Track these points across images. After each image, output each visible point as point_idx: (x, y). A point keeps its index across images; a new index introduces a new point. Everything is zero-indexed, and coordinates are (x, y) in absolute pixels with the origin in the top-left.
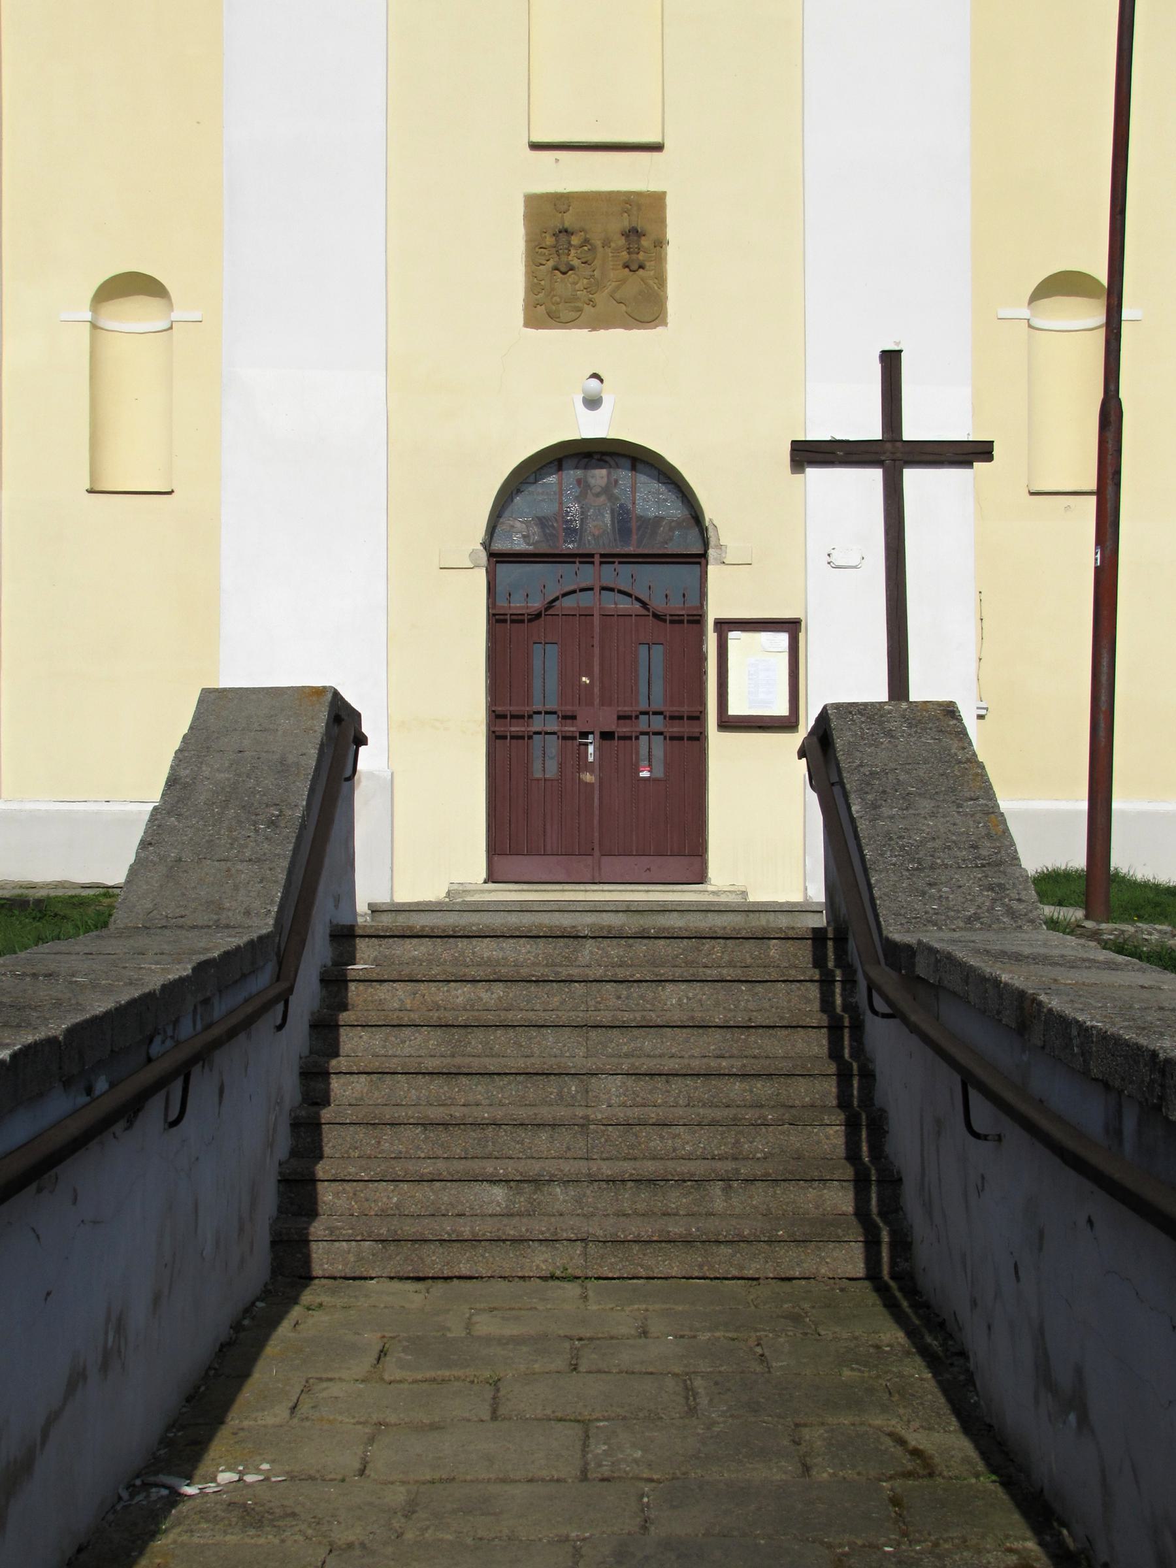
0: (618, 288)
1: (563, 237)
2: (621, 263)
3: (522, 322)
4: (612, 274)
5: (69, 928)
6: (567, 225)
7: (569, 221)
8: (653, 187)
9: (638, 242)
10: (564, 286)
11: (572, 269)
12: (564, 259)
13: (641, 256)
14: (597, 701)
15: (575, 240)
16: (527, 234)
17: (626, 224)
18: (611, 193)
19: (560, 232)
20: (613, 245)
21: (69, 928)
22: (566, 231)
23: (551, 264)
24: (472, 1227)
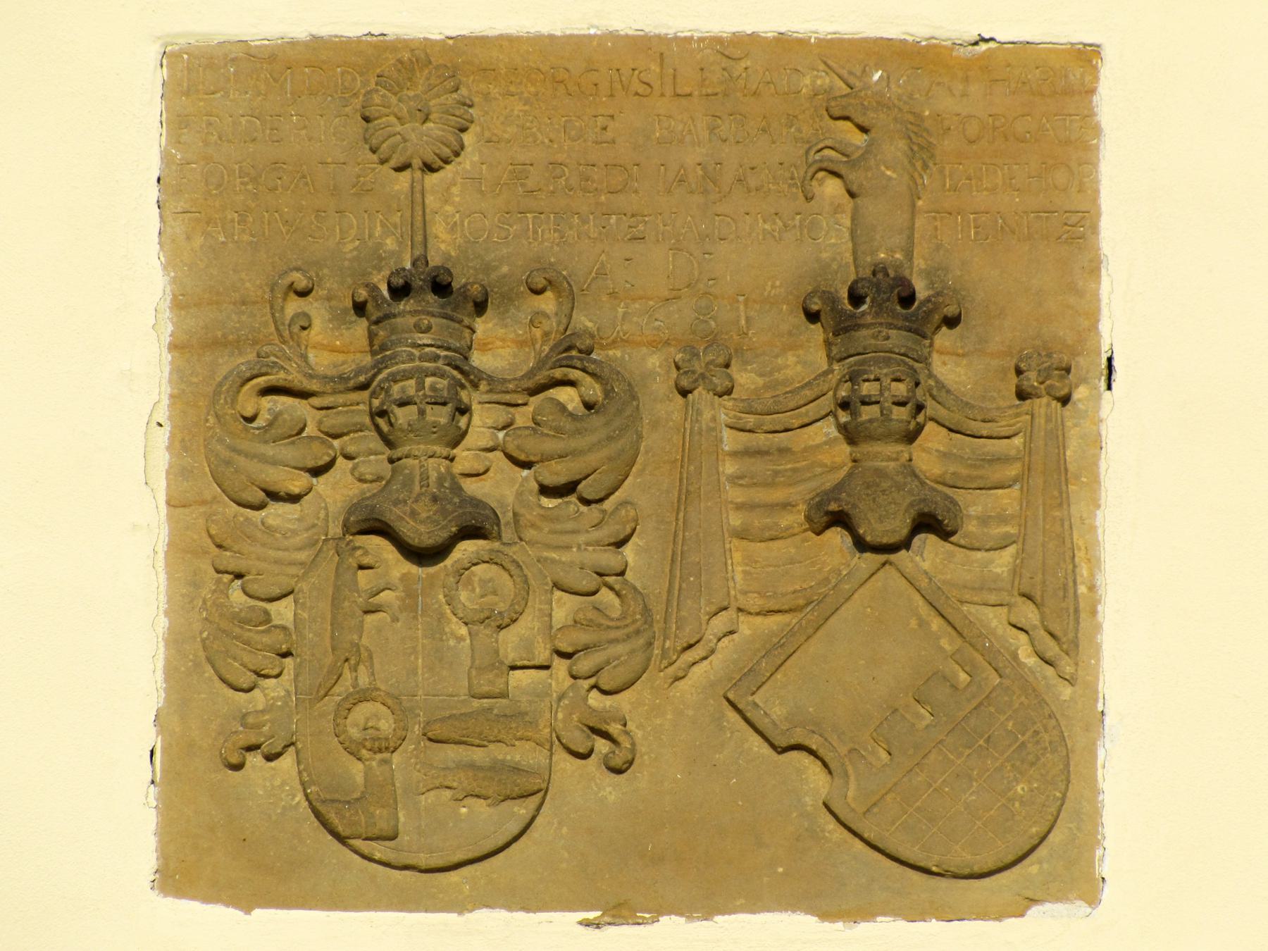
0: (779, 652)
1: (419, 325)
2: (801, 493)
3: (141, 848)
4: (739, 568)
5: (368, 744)
6: (444, 245)
7: (457, 220)
8: (134, 142)
9: (913, 368)
10: (425, 633)
12: (425, 461)
13: (932, 452)
15: (498, 347)
16: (181, 303)
18: (732, 50)
19: (400, 291)
20: (745, 378)
21: (368, 744)
22: (441, 287)
23: (336, 492)
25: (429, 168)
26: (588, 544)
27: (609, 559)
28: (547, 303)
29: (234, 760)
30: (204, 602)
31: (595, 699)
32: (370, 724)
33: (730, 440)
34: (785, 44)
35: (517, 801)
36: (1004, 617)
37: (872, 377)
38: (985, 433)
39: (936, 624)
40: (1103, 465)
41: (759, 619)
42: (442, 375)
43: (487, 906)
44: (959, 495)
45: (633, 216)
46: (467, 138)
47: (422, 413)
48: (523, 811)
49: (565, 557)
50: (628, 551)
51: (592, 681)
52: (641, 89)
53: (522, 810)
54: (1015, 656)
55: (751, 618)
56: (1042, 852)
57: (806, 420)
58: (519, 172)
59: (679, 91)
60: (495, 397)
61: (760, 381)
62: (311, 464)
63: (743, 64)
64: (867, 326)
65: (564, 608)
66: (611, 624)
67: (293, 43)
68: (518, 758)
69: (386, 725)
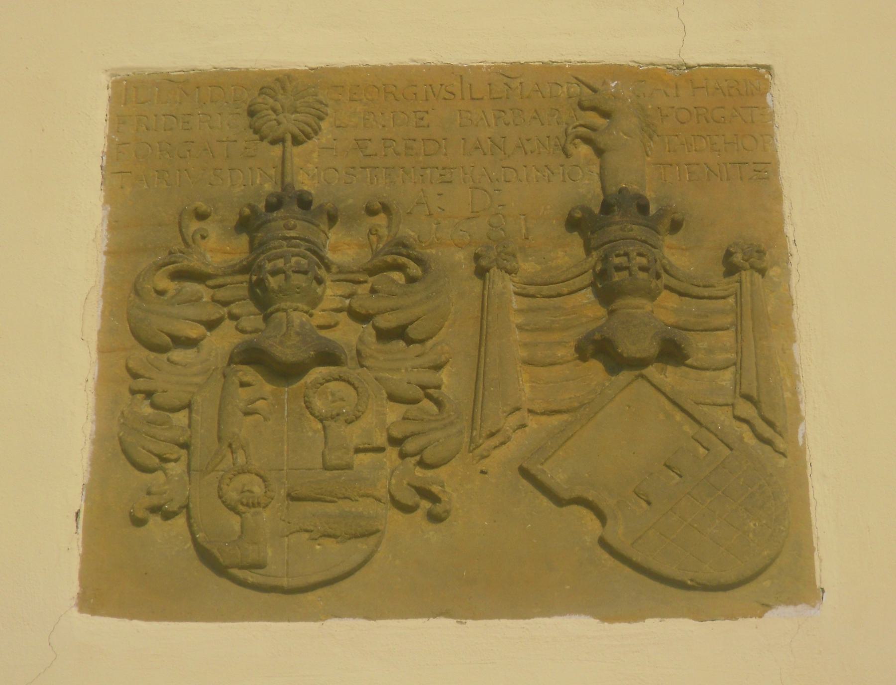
2: (572, 337)
3: (68, 581)
4: (525, 386)
6: (305, 183)
8: (706, 41)
11: (328, 356)
14: (313, 135)
15: (344, 247)
16: (114, 225)
17: (587, 188)
22: (304, 202)
23: (223, 341)
24: (568, 89)
25: (296, 142)
26: (413, 368)
27: (428, 377)
28: (381, 220)
29: (140, 514)
30: (122, 413)
31: (419, 472)
32: (246, 488)
33: (516, 303)
34: (548, 68)
35: (361, 539)
36: (730, 414)
37: (622, 252)
38: (706, 294)
39: (679, 416)
40: (795, 316)
41: (543, 419)
42: (304, 257)
43: (336, 617)
44: (690, 335)
45: (444, 169)
46: (324, 125)
47: (287, 278)
48: (365, 547)
49: (396, 377)
50: (444, 376)
51: (418, 458)
52: (447, 96)
53: (362, 546)
54: (741, 439)
55: (538, 417)
56: (773, 570)
57: (574, 288)
58: (360, 145)
59: (474, 96)
60: (343, 276)
61: (538, 267)
62: (205, 318)
63: (519, 81)
64: (617, 223)
65: (394, 413)
66: (433, 418)
67: (202, 73)
68: (361, 509)
69: (258, 490)
